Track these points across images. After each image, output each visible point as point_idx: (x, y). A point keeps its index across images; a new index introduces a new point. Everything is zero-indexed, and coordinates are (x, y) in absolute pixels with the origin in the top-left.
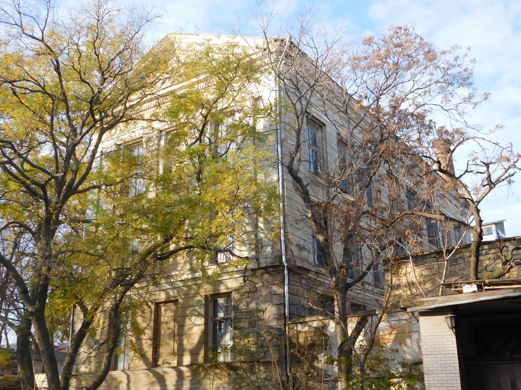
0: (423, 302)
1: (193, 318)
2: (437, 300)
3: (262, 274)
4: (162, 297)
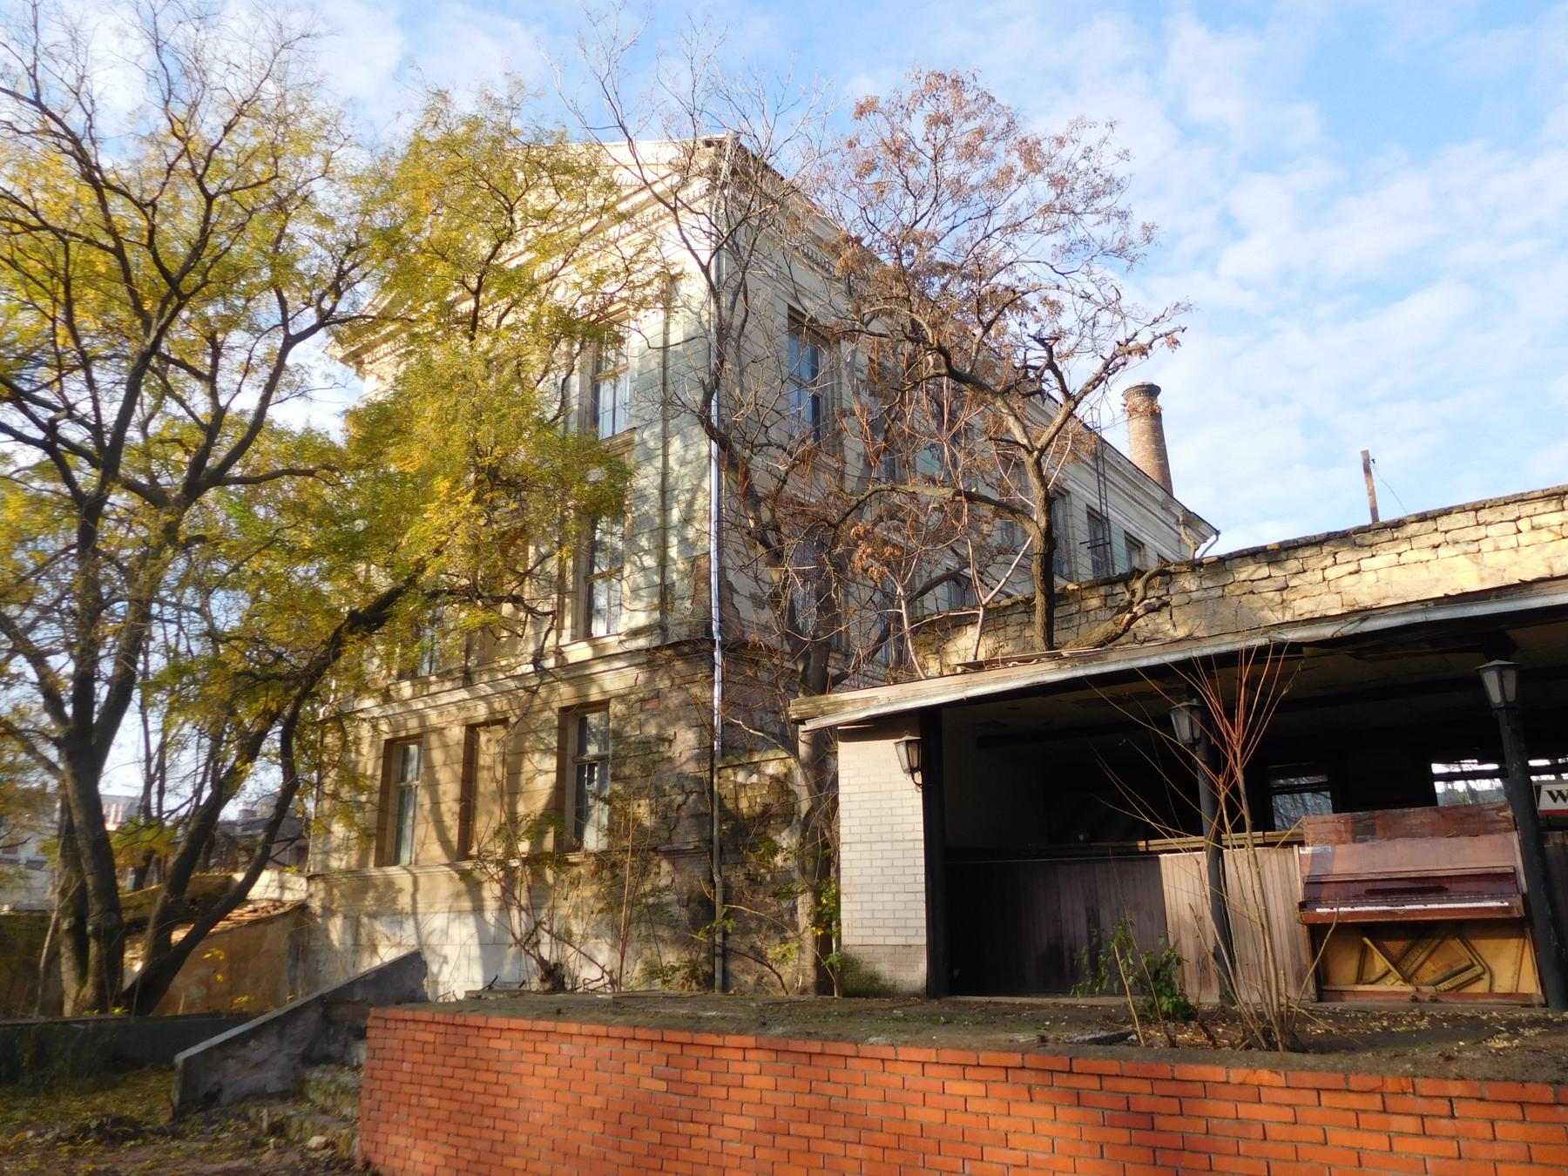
0: (843, 704)
1: (537, 757)
2: (875, 698)
3: (669, 661)
4: (481, 712)
